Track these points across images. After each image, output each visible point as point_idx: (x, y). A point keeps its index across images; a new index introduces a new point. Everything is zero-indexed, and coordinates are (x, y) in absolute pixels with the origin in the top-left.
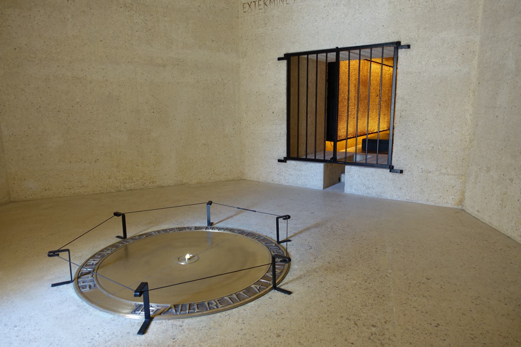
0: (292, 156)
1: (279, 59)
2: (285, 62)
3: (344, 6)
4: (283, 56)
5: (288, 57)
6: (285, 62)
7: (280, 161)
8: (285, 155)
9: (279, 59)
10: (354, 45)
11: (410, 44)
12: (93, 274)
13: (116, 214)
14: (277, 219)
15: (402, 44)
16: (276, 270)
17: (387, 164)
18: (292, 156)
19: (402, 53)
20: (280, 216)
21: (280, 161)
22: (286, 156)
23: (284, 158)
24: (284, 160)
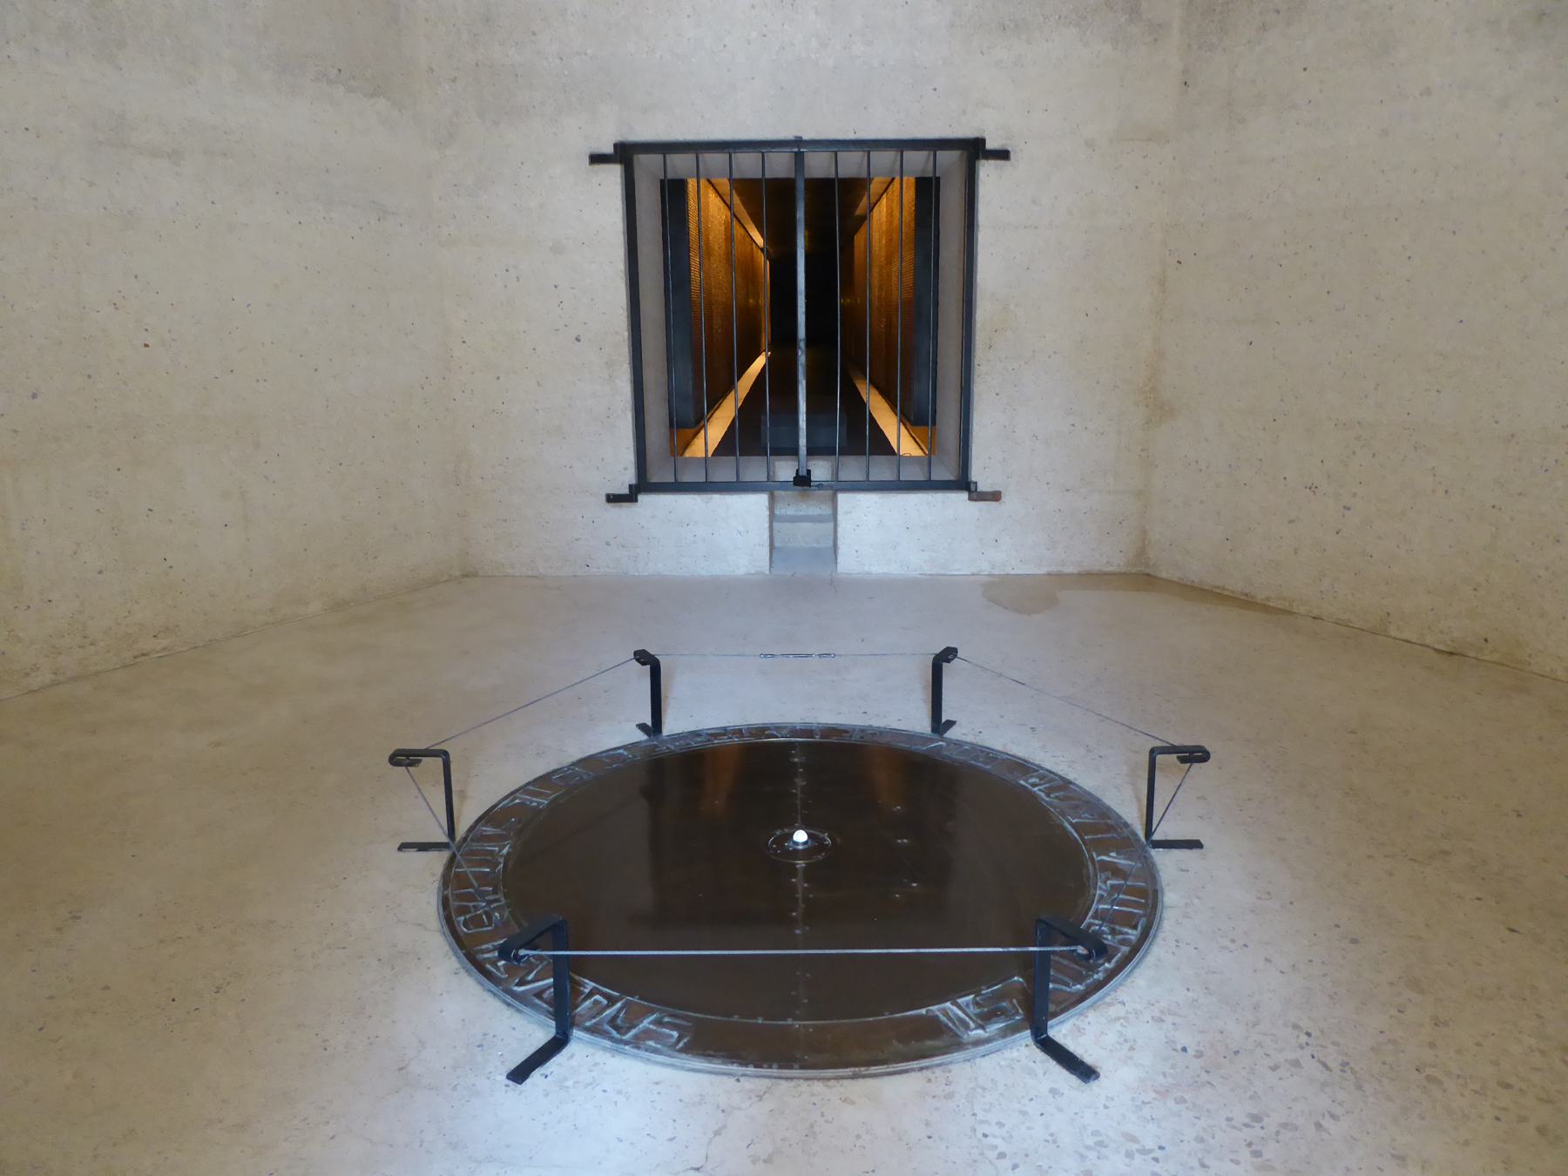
0: (655, 477)
1: (597, 159)
2: (615, 172)
3: (817, 13)
4: (609, 150)
5: (625, 154)
6: (615, 172)
7: (613, 499)
8: (629, 477)
9: (597, 159)
10: (851, 136)
11: (1010, 149)
12: (1240, 1130)
13: (404, 758)
14: (1153, 752)
15: (990, 145)
16: (1071, 920)
17: (704, 480)
18: (655, 477)
19: (987, 171)
20: (1174, 746)
21: (613, 499)
22: (634, 481)
23: (630, 486)
24: (630, 497)
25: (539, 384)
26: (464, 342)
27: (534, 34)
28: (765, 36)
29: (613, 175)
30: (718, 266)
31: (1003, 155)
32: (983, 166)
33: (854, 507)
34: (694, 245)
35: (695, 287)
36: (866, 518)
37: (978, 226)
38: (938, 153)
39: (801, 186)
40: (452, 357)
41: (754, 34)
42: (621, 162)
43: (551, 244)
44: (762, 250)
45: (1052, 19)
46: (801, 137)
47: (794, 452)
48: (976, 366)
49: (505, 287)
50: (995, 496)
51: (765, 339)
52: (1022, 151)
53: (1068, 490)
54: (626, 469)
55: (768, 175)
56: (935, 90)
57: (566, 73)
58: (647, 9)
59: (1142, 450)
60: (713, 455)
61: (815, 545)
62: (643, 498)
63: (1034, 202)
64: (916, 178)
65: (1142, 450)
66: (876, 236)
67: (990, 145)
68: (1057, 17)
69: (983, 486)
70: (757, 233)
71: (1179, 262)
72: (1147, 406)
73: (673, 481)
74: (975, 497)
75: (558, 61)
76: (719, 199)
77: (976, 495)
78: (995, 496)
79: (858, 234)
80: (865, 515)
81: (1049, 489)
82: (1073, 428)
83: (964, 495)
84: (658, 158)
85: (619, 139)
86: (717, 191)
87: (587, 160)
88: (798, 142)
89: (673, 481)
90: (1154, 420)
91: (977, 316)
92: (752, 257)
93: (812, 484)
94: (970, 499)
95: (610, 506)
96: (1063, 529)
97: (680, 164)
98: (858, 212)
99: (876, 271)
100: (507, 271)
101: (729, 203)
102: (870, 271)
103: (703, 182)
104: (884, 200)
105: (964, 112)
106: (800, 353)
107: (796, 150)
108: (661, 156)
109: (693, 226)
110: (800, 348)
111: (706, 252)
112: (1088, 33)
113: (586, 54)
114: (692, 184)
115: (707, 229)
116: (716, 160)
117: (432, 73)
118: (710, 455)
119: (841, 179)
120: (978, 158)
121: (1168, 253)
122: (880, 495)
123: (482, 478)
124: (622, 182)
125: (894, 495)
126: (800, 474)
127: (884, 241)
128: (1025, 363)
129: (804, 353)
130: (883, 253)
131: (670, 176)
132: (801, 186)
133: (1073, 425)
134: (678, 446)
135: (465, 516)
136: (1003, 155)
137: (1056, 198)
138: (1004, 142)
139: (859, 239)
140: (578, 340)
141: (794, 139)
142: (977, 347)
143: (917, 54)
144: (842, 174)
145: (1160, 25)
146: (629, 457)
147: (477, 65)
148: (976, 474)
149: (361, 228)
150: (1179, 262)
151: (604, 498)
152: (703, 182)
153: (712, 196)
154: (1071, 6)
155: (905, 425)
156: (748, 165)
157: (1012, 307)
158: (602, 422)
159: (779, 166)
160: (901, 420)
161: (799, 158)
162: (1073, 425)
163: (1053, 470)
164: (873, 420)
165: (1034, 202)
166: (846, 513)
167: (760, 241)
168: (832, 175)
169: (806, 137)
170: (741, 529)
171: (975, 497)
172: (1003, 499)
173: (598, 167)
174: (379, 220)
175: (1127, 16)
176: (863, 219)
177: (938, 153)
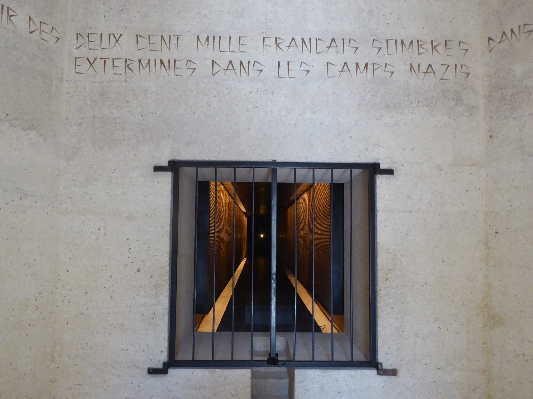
1: (158, 169)
3: (286, 97)
7: (152, 371)
8: (164, 357)
9: (158, 169)
10: (304, 160)
15: (382, 167)
19: (381, 180)
21: (152, 371)
25: (112, 297)
26: (68, 271)
27: (128, 102)
28: (256, 107)
29: (167, 178)
30: (224, 226)
31: (390, 172)
32: (379, 177)
33: (305, 378)
34: (212, 215)
35: (211, 236)
36: (312, 386)
37: (377, 210)
38: (334, 170)
39: (274, 187)
40: (59, 280)
41: (251, 106)
42: (172, 171)
43: (127, 215)
44: (244, 213)
45: (414, 103)
46: (276, 160)
47: (265, 328)
48: (379, 291)
49: (97, 239)
50: (393, 372)
51: (244, 253)
52: (400, 170)
53: (439, 369)
54: (162, 352)
55: (255, 181)
56: (351, 137)
57: (144, 123)
58: (192, 92)
59: (483, 344)
60: (217, 331)
61: (277, 393)
62: (172, 371)
63: (408, 197)
64: (343, 184)
65: (483, 344)
66: (301, 210)
67: (382, 167)
68: (417, 102)
69: (386, 365)
70: (243, 206)
71: (497, 232)
72: (484, 316)
73: (191, 359)
74: (382, 373)
75: (140, 117)
76: (226, 191)
77: (382, 371)
78: (393, 372)
79: (290, 208)
80: (312, 384)
81: (427, 368)
82: (439, 329)
83: (374, 372)
84: (194, 169)
85: (172, 158)
86: (225, 188)
87: (152, 169)
88: (274, 163)
89: (191, 359)
90: (489, 325)
91: (378, 261)
92: (240, 217)
93: (279, 363)
94: (378, 374)
95: (150, 376)
96: (437, 394)
97: (206, 173)
98: (292, 198)
99: (302, 227)
100: (99, 229)
101: (233, 196)
102: (298, 225)
103: (219, 184)
104: (307, 194)
105: (367, 149)
106: (273, 282)
107: (273, 167)
108: (196, 168)
109: (212, 205)
110: (273, 279)
111: (219, 217)
112: (434, 110)
113: (156, 114)
114: (213, 184)
115: (220, 206)
116: (226, 172)
117: (68, 120)
118: (215, 331)
119: (297, 183)
120: (376, 174)
121: (488, 227)
122: (321, 371)
123: (69, 357)
124: (172, 181)
125: (330, 370)
126: (272, 356)
127: (307, 213)
128: (408, 289)
129: (275, 281)
130: (307, 218)
131: (200, 179)
132: (274, 187)
133: (439, 328)
134: (197, 322)
135: (54, 382)
136: (390, 172)
137: (421, 196)
138: (390, 165)
139: (290, 211)
140: (138, 271)
141: (271, 161)
142: (378, 279)
143: (340, 119)
144: (256, 180)
145: (473, 107)
146: (164, 344)
147: (94, 117)
148: (381, 358)
149: (7, 204)
150: (497, 232)
151: (146, 371)
152: (219, 184)
153: (223, 191)
154: (424, 97)
155: (316, 302)
156: (244, 175)
157: (399, 256)
158: (149, 322)
159: (261, 175)
160: (314, 301)
161: (274, 172)
162: (439, 328)
163: (429, 356)
164: (298, 296)
165: (408, 197)
166: (300, 382)
167: (243, 209)
168: (251, 180)
169: (278, 160)
170: (233, 392)
171: (382, 373)
172: (399, 374)
173: (158, 173)
174: (21, 199)
175: (455, 103)
176: (293, 202)
177: (334, 170)
